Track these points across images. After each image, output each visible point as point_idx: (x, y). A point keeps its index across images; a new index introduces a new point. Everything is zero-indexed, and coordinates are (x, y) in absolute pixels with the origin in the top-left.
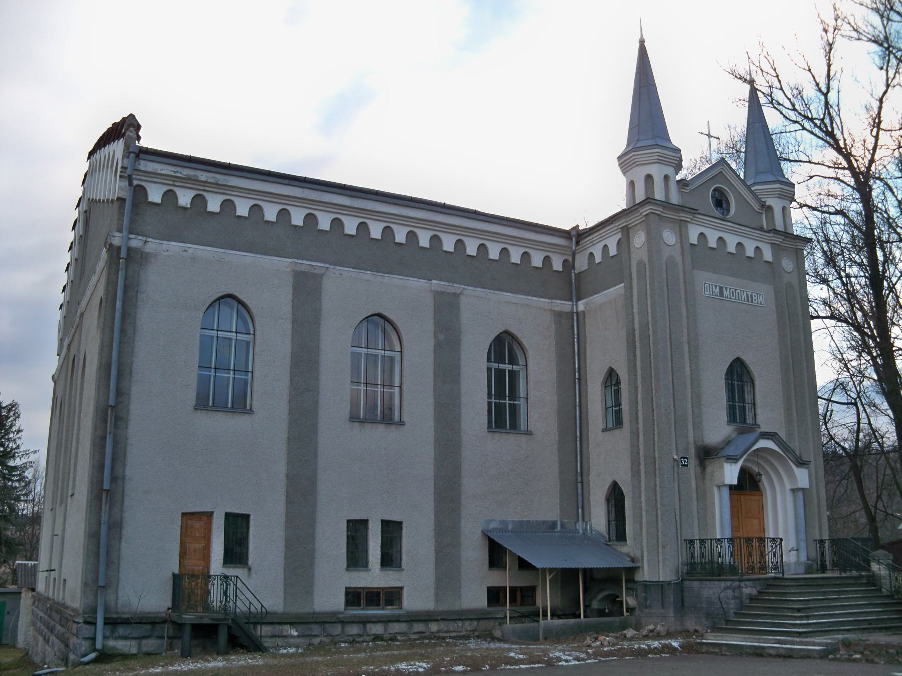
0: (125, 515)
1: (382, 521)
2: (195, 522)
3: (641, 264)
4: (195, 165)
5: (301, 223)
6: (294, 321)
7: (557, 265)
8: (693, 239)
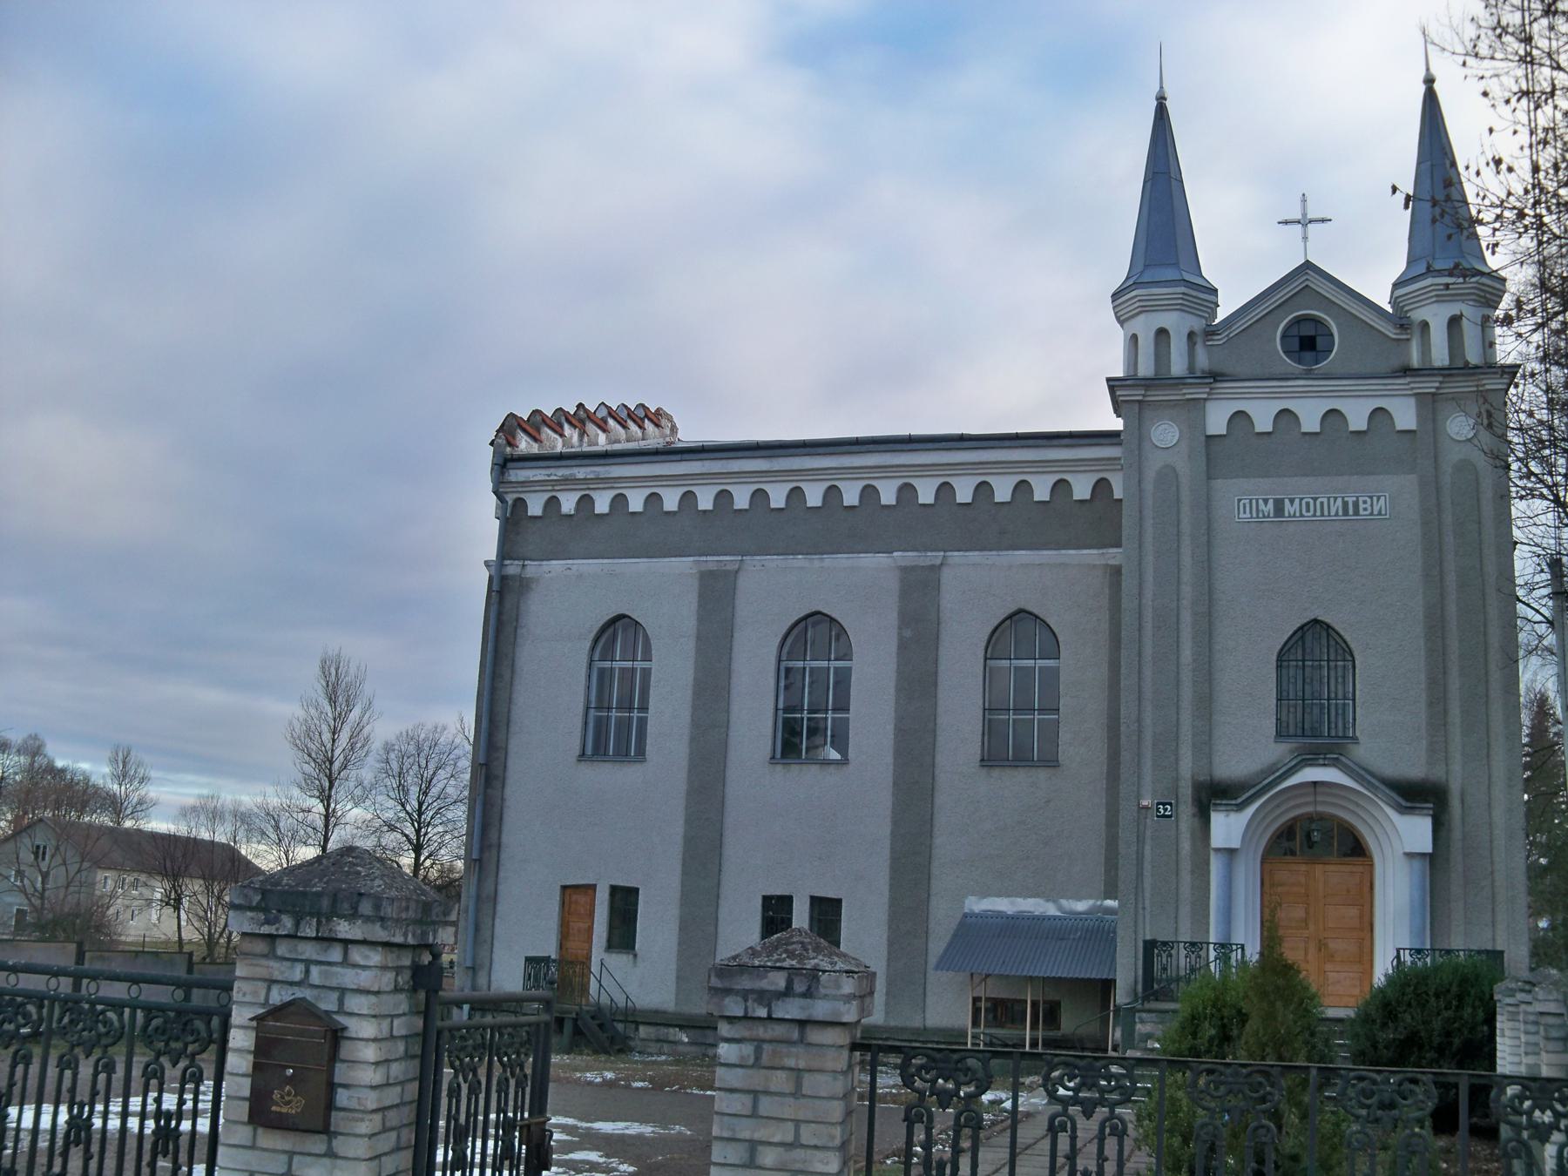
0: (500, 888)
1: (812, 898)
2: (574, 896)
5: (930, 500)
6: (698, 638)
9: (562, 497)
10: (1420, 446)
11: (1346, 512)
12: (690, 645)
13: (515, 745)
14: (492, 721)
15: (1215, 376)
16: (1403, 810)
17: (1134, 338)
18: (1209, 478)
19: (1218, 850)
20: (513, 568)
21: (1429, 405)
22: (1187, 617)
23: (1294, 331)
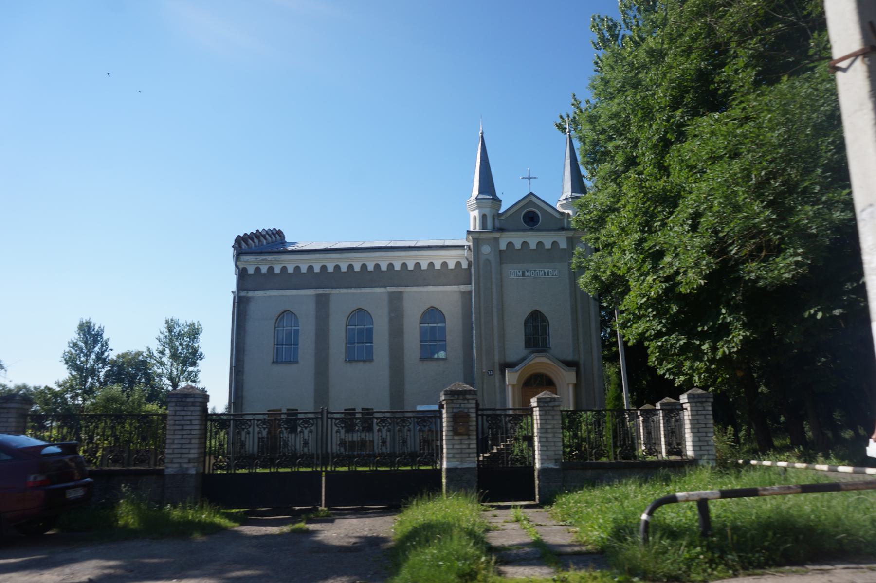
8: (503, 246)
18: (501, 263)
20: (243, 294)
22: (495, 310)
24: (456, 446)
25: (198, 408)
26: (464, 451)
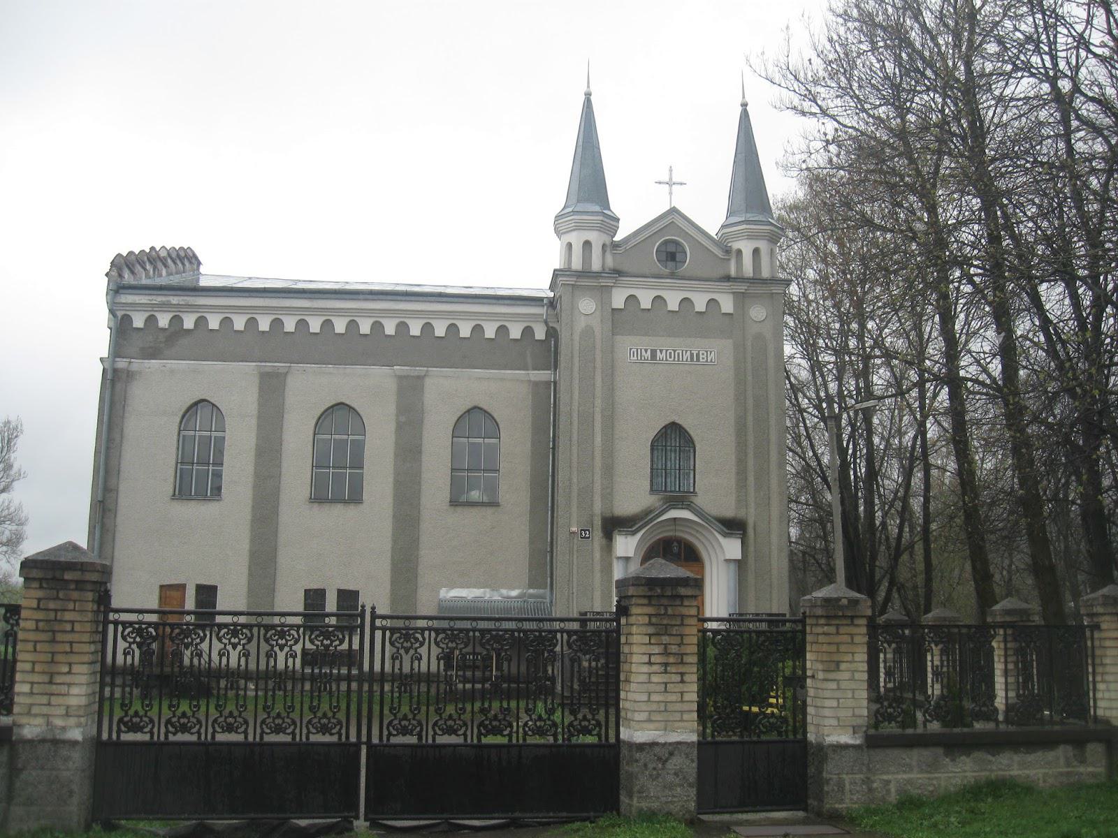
3: (588, 332)
4: (165, 292)
6: (259, 417)
7: (540, 334)
9: (159, 315)
10: (733, 324)
11: (692, 359)
12: (254, 422)
13: (123, 487)
14: (107, 472)
15: (618, 273)
16: (725, 535)
17: (570, 245)
19: (619, 558)
21: (741, 298)
22: (598, 417)
23: (663, 249)
24: (655, 697)
25: (90, 596)
26: (670, 707)
